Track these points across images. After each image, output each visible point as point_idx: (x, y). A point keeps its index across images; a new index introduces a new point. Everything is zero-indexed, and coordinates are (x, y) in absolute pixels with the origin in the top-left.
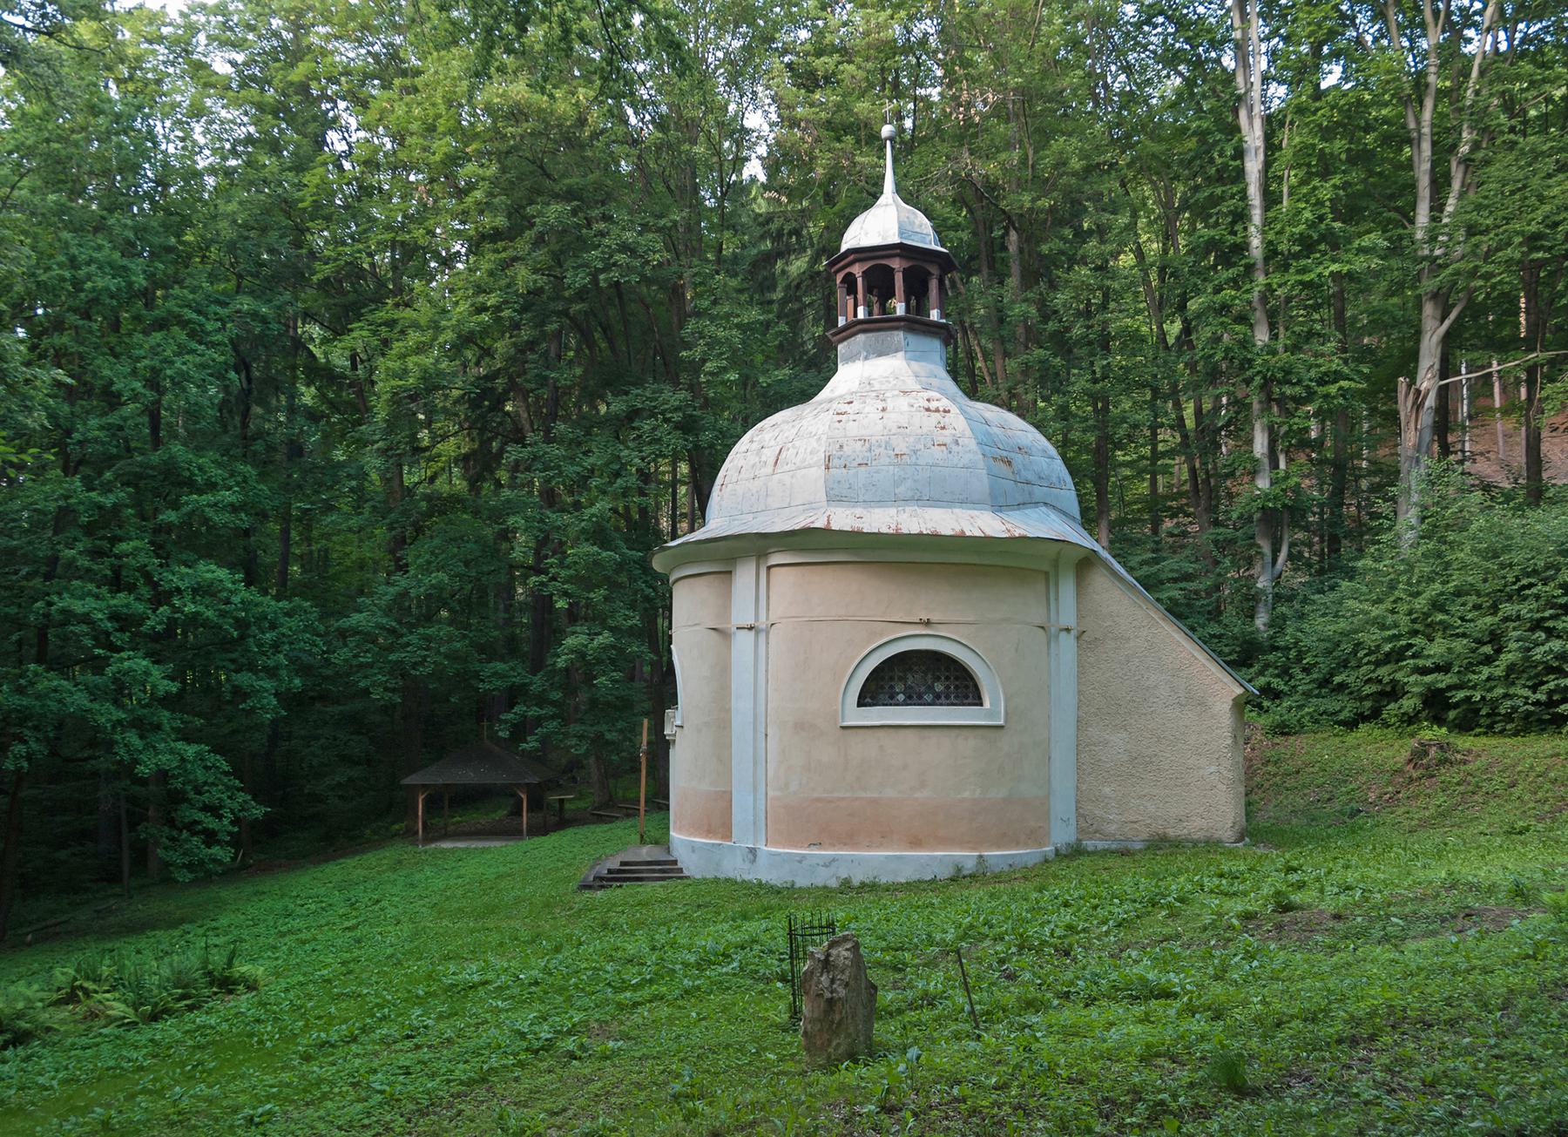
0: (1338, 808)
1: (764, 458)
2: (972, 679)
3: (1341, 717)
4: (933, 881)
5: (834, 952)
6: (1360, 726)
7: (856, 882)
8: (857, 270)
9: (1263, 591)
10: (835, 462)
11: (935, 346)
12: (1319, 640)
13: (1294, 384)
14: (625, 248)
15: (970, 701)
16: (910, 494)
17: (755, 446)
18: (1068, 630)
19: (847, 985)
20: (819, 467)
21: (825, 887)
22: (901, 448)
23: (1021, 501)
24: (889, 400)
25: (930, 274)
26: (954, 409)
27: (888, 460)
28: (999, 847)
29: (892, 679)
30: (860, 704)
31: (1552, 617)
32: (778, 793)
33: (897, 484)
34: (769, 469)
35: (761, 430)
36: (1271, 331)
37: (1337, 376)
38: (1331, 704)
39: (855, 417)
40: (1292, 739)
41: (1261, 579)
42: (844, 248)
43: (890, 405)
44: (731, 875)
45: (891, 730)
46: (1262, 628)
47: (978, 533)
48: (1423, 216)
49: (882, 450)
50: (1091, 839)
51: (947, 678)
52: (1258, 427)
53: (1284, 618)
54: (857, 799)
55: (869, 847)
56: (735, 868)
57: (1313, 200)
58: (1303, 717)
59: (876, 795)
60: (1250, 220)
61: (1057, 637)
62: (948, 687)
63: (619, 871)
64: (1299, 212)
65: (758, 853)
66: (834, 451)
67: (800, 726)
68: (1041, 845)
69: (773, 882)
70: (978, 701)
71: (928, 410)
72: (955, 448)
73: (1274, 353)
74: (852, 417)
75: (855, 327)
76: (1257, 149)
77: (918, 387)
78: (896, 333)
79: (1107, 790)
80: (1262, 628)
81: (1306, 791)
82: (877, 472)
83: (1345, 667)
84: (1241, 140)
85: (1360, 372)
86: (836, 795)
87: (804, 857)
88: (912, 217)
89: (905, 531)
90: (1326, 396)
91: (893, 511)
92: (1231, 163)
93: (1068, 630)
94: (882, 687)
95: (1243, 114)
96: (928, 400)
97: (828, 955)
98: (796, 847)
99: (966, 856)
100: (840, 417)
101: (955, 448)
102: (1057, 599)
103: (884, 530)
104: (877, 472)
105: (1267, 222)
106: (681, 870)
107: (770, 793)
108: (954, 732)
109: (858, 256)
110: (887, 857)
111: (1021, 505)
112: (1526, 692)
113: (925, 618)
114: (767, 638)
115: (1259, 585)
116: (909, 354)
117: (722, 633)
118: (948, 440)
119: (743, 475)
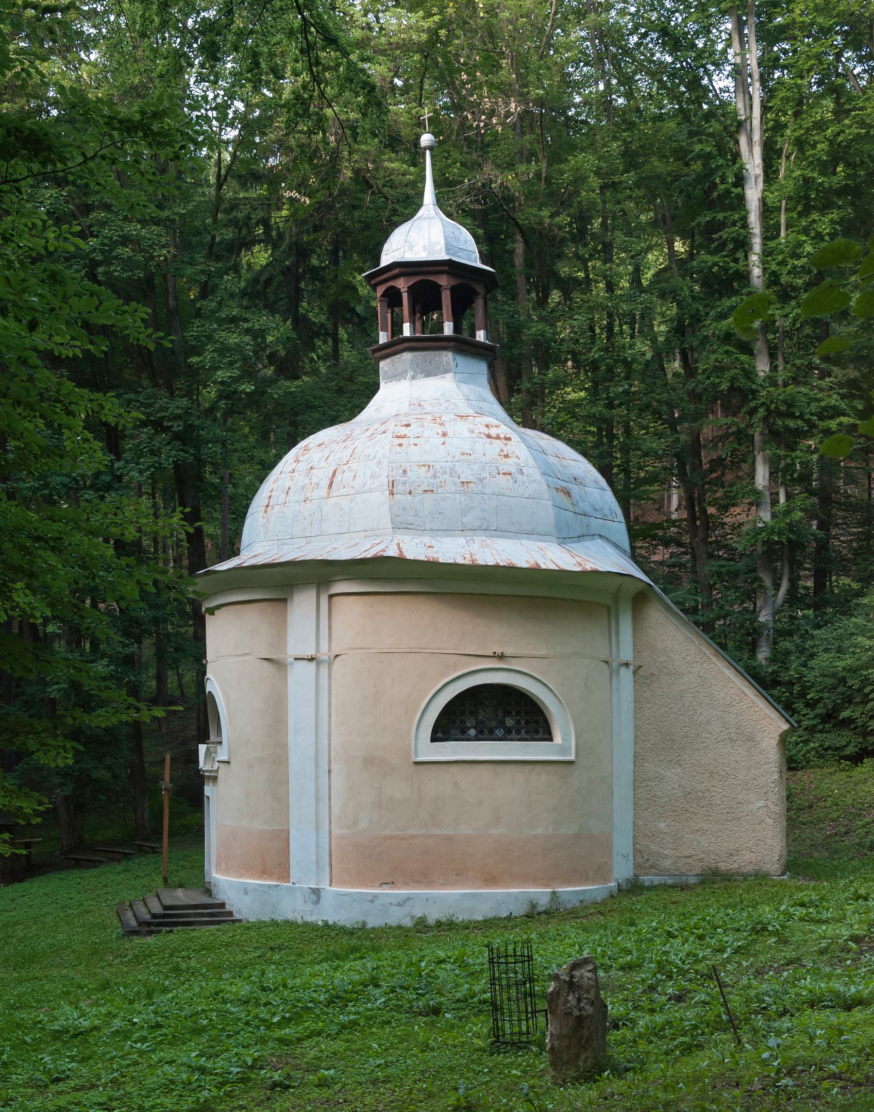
0: (857, 841)
1: (315, 480)
2: (542, 713)
3: (848, 751)
4: (509, 918)
5: (577, 973)
6: (865, 760)
7: (431, 921)
8: (402, 284)
9: (764, 625)
10: (399, 488)
11: (481, 368)
12: (823, 675)
13: (797, 417)
14: (125, 240)
15: (540, 736)
17: (302, 466)
18: (627, 665)
19: (593, 1003)
21: (400, 927)
23: (580, 533)
24: (447, 424)
25: (477, 293)
26: (515, 437)
27: (453, 488)
28: (570, 883)
29: (463, 713)
30: (434, 739)
32: (345, 831)
34: (323, 491)
35: (306, 449)
36: (771, 363)
37: (837, 412)
38: (834, 739)
39: (417, 441)
40: (800, 774)
41: (763, 613)
42: (386, 260)
43: (449, 429)
44: (290, 917)
45: (466, 766)
46: (764, 662)
47: (553, 567)
49: (447, 476)
50: (647, 874)
51: (518, 713)
52: (759, 459)
53: (788, 653)
54: (431, 836)
55: (444, 885)
57: (813, 233)
58: (808, 752)
59: (449, 832)
60: (751, 249)
61: (618, 671)
62: (518, 722)
63: (165, 916)
64: (800, 244)
65: (322, 893)
66: (397, 475)
67: (369, 762)
68: (606, 880)
69: (342, 923)
70: (548, 736)
71: (489, 436)
73: (774, 384)
74: (413, 441)
75: (398, 345)
76: (757, 177)
77: (470, 412)
78: (445, 353)
79: (662, 825)
80: (764, 662)
81: (822, 825)
82: (444, 499)
83: (850, 702)
84: (742, 168)
85: (854, 408)
87: (376, 896)
88: (457, 232)
89: (481, 562)
90: (827, 432)
91: (462, 541)
92: (733, 190)
93: (627, 665)
94: (454, 722)
95: (743, 140)
96: (487, 426)
97: (572, 977)
98: (366, 886)
99: (540, 893)
100: (401, 441)
101: (519, 477)
102: (617, 634)
103: (460, 561)
104: (444, 499)
105: (766, 253)
106: (231, 914)
107: (336, 832)
108: (528, 768)
109: (403, 270)
110: (462, 895)
111: (581, 537)
113: (499, 652)
114: (330, 670)
115: (762, 619)
116: (458, 376)
117: (277, 664)
118: (513, 470)
119: (291, 496)
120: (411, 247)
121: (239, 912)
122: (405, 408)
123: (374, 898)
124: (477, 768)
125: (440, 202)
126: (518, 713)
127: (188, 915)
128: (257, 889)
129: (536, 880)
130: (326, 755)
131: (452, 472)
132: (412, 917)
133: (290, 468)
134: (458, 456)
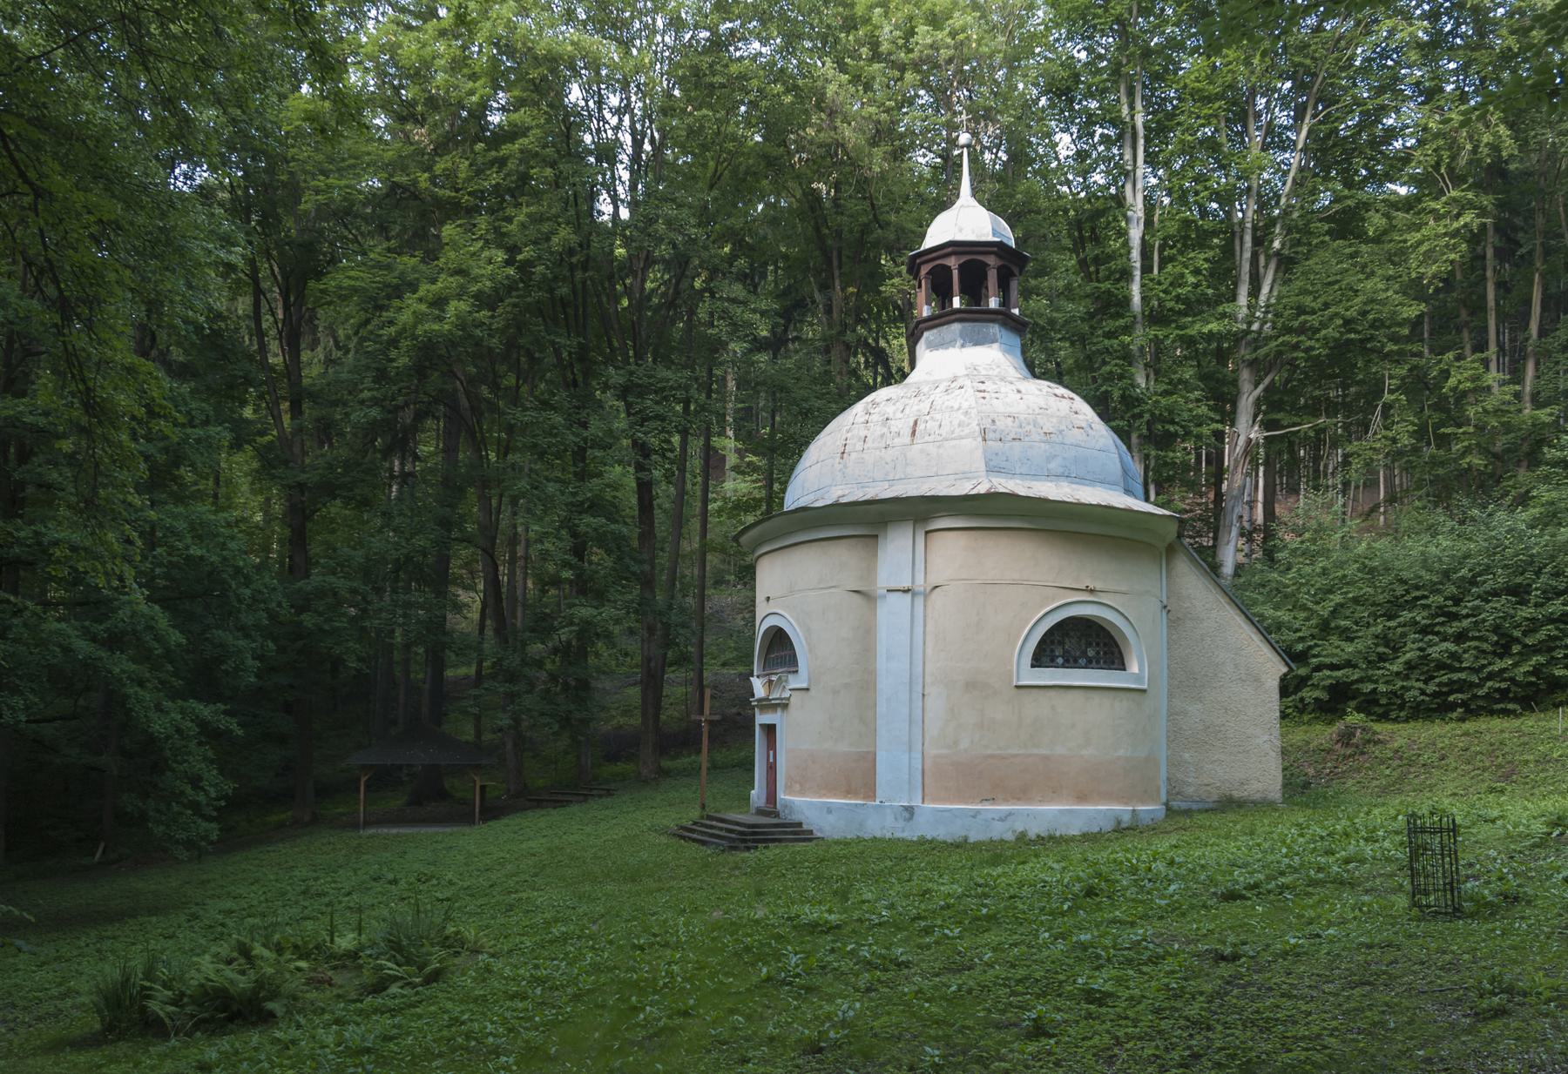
1: (894, 429)
10: (990, 435)
16: (1060, 470)
20: (975, 439)
22: (1048, 428)
30: (1033, 666)
31: (1442, 624)
33: (1049, 460)
34: (908, 440)
35: (874, 403)
44: (878, 834)
45: (1062, 691)
48: (1243, 299)
51: (1098, 644)
55: (1041, 802)
56: (880, 823)
59: (1046, 752)
62: (1098, 653)
66: (987, 424)
69: (941, 838)
72: (1090, 432)
76: (1138, 219)
79: (1187, 756)
86: (1010, 751)
87: (978, 812)
95: (1128, 187)
98: (966, 803)
101: (1090, 432)
104: (1031, 447)
106: (811, 832)
110: (1060, 811)
112: (1420, 685)
113: (1091, 587)
117: (867, 596)
118: (1084, 425)
120: (961, 230)
121: (821, 830)
122: (961, 372)
123: (976, 814)
124: (1071, 694)
125: (976, 192)
126: (1098, 644)
127: (773, 833)
128: (841, 807)
129: (1108, 797)
130: (921, 680)
131: (1035, 423)
132: (1014, 831)
133: (863, 420)
134: (1037, 411)
